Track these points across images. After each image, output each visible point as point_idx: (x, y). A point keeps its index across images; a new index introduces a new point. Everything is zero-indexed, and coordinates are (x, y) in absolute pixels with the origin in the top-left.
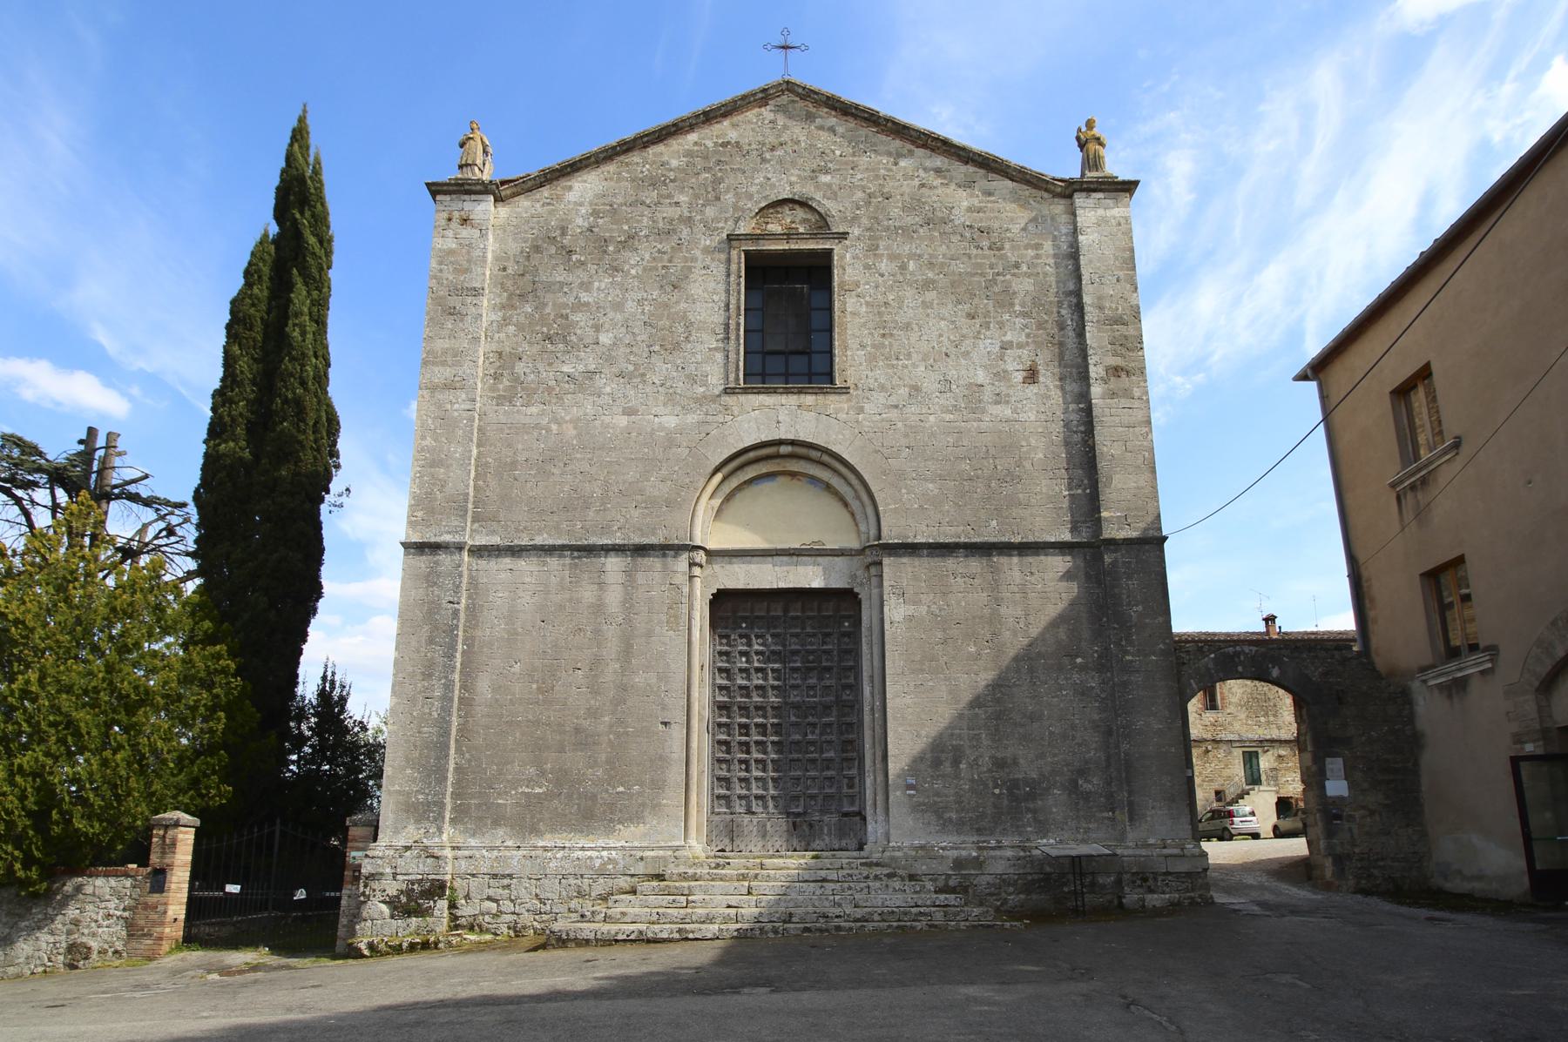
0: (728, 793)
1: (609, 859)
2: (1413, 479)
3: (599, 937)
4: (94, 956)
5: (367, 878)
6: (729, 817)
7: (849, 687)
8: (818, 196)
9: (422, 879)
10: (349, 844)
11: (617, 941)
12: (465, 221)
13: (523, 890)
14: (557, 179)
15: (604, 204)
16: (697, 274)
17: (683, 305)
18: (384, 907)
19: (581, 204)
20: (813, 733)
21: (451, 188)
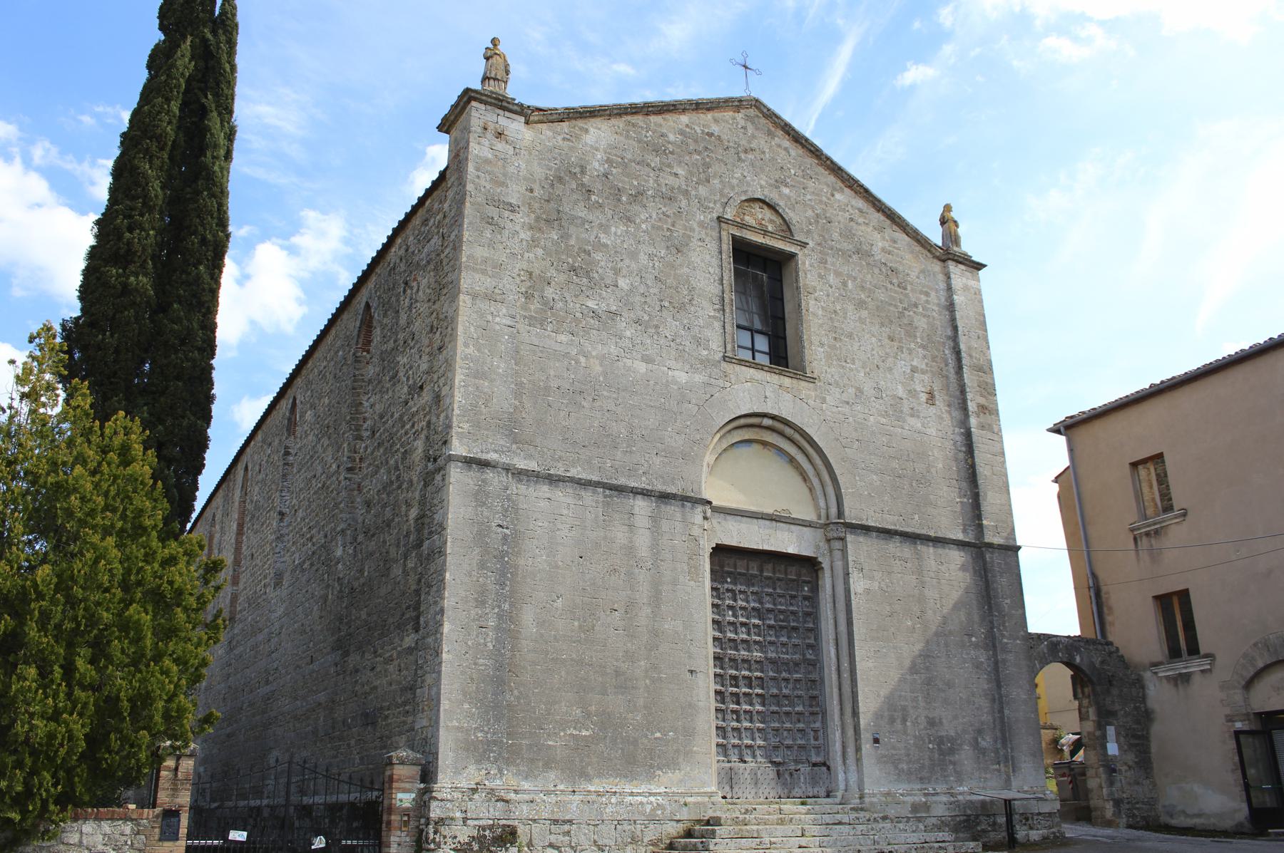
0: (725, 742)
1: (658, 804)
2: (1148, 529)
5: (436, 823)
6: (729, 765)
10: (395, 785)
12: (499, 135)
15: (616, 155)
16: (695, 243)
17: (686, 270)
20: (786, 688)
21: (489, 100)
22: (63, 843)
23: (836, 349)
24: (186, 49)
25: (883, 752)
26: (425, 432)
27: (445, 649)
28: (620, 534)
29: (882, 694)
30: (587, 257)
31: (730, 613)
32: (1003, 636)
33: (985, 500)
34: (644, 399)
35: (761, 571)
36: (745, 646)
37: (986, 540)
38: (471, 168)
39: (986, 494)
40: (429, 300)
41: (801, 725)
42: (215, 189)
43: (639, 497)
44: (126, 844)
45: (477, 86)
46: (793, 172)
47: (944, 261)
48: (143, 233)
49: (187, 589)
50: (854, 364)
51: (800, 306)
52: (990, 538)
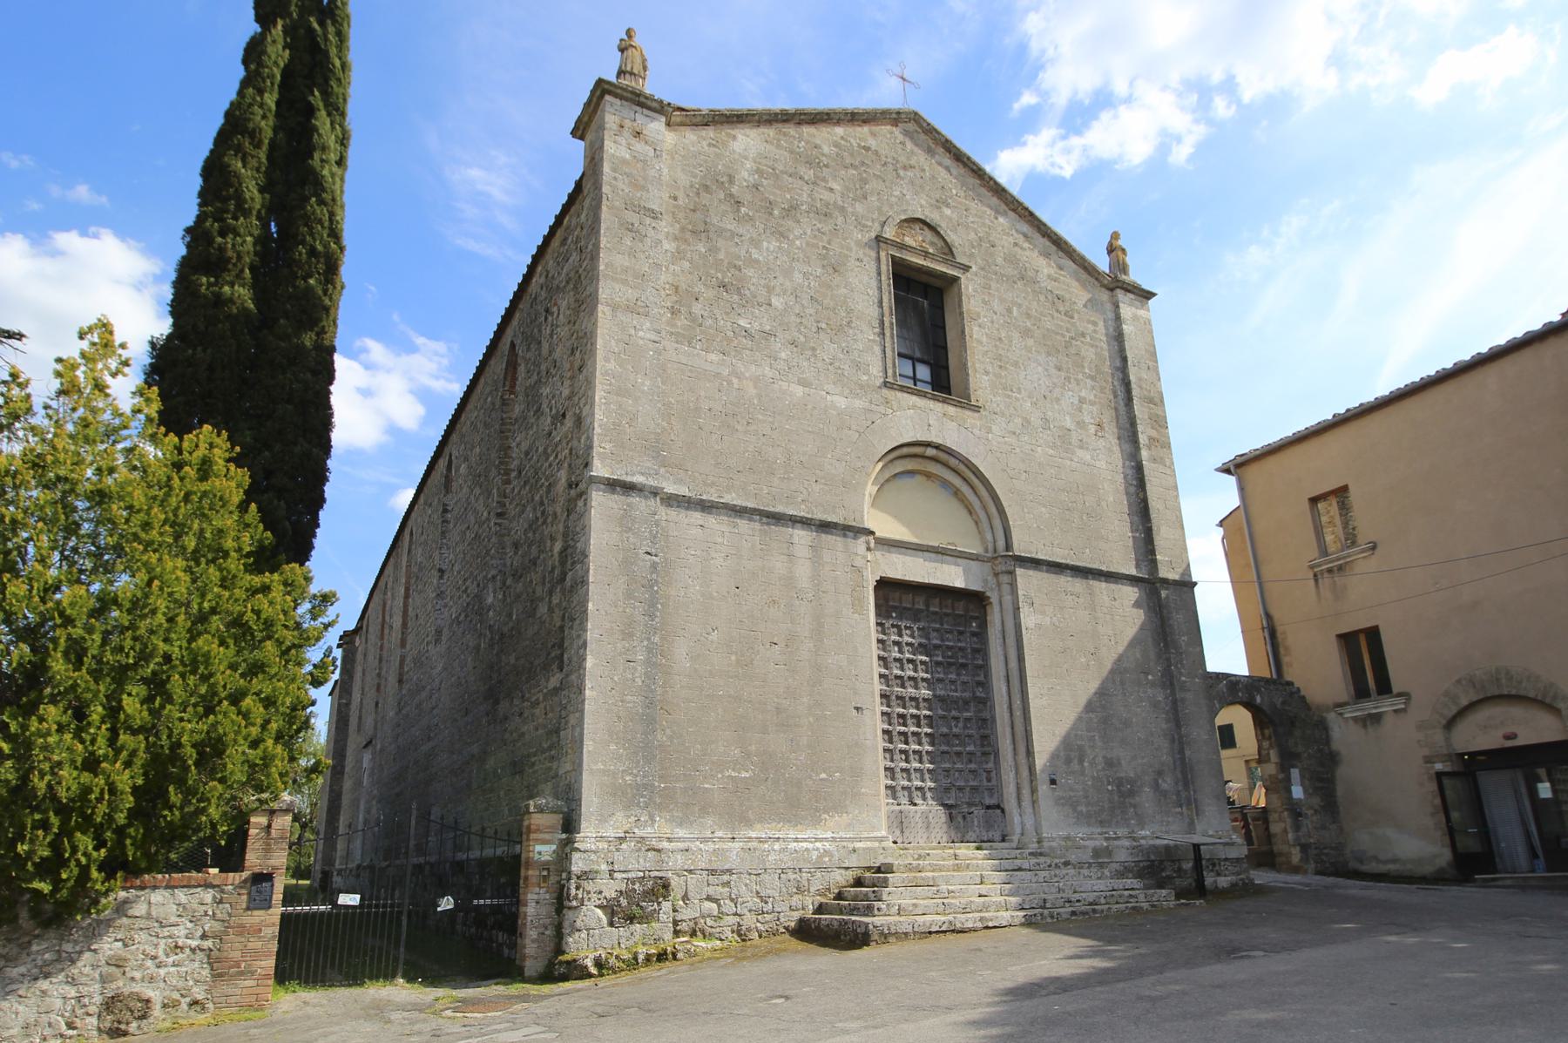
3: (916, 930)
4: (157, 1011)
6: (898, 808)
8: (943, 225)
9: (644, 878)
10: (532, 836)
11: (930, 933)
14: (722, 123)
15: (766, 165)
16: (852, 263)
18: (599, 912)
19: (746, 158)
20: (956, 727)
21: (625, 94)
22: (126, 916)
25: (1061, 794)
26: (568, 460)
27: (588, 684)
30: (737, 272)
31: (896, 649)
32: (1181, 674)
35: (928, 606)
36: (912, 683)
37: (1161, 575)
38: (606, 168)
41: (973, 766)
42: (324, 195)
43: (799, 525)
44: (206, 915)
46: (954, 192)
47: (1112, 290)
49: (279, 620)
50: (1020, 393)
51: (963, 332)
52: (1165, 572)
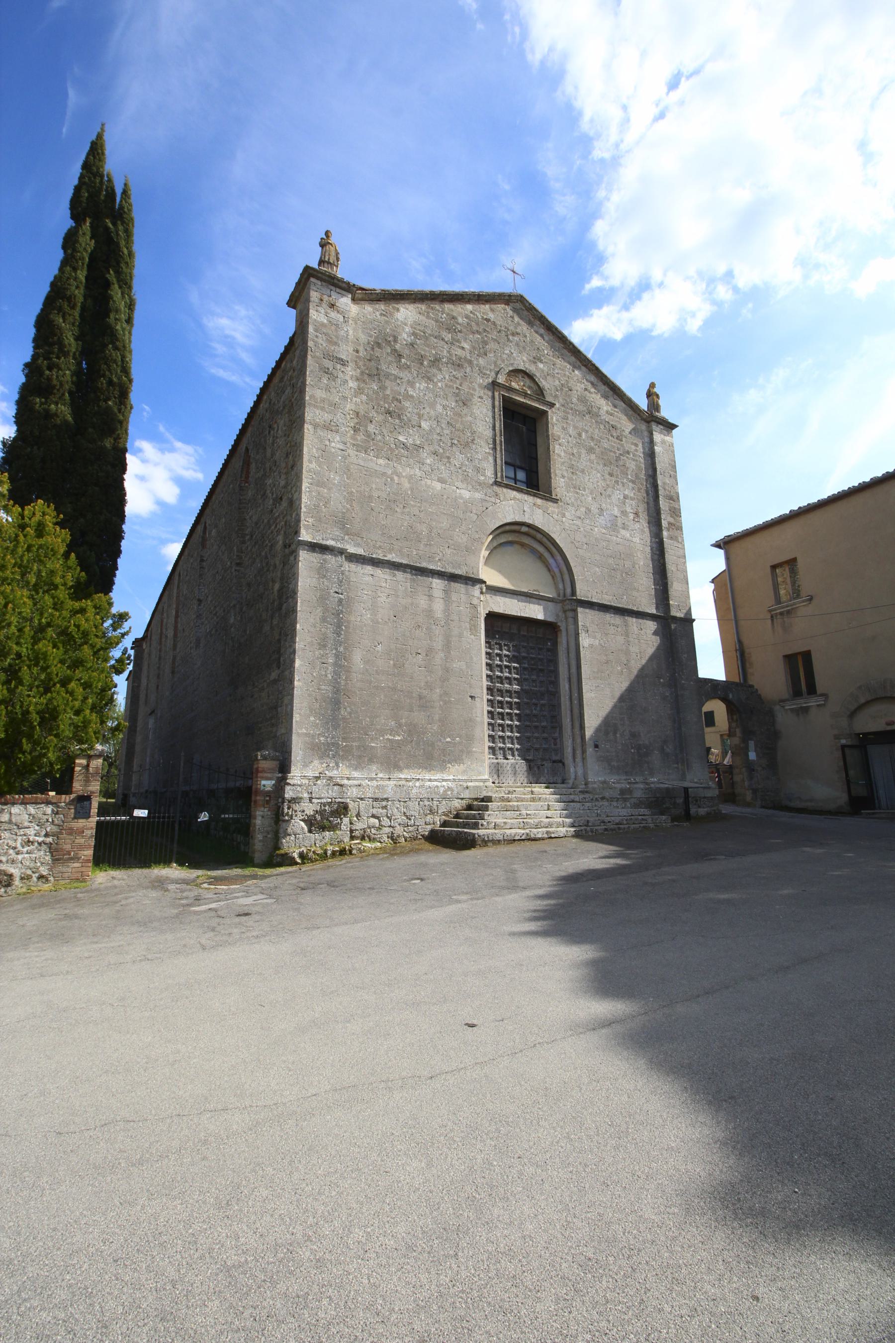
0: (494, 745)
3: (505, 838)
4: (17, 882)
5: (289, 802)
6: (496, 761)
7: (552, 682)
9: (331, 802)
11: (514, 840)
13: (396, 810)
14: (390, 300)
15: (420, 330)
16: (476, 399)
18: (302, 824)
20: (535, 709)
21: (324, 277)
23: (573, 480)
24: (87, 229)
27: (296, 678)
28: (422, 602)
29: (600, 715)
33: (671, 587)
34: (440, 508)
36: (508, 681)
38: (311, 329)
39: (672, 583)
40: (285, 435)
41: (545, 735)
45: (315, 265)
46: (546, 352)
48: (60, 372)
50: (585, 491)
51: (549, 448)
52: (675, 613)
